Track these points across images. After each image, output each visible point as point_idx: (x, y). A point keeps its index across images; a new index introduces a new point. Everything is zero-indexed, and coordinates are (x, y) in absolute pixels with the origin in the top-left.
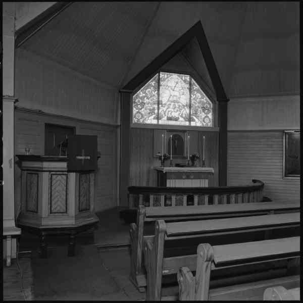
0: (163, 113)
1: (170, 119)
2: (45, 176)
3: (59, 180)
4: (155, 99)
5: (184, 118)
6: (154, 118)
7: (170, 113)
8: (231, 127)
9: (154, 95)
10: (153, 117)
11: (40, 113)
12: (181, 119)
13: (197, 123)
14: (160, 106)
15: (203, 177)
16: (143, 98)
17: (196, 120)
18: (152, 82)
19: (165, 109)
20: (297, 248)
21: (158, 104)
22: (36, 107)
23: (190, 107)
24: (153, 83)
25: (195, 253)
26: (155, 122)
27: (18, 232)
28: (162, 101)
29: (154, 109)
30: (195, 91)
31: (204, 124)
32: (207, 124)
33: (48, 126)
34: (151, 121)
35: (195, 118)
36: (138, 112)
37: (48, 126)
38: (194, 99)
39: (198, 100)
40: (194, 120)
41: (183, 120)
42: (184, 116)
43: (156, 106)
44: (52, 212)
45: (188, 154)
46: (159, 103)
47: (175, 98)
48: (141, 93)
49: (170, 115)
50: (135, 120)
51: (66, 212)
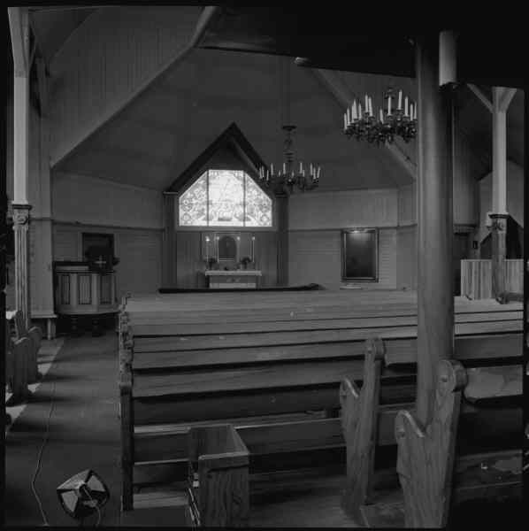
0: (213, 213)
1: (220, 219)
2: (74, 278)
3: (84, 280)
4: (205, 199)
6: (204, 219)
8: (292, 226)
12: (235, 219)
13: (253, 223)
16: (190, 199)
18: (200, 181)
20: (516, 389)
21: (208, 204)
23: (244, 205)
24: (202, 182)
26: (204, 224)
27: (55, 316)
29: (203, 210)
30: (249, 188)
32: (265, 224)
33: (85, 235)
34: (200, 222)
36: (185, 214)
37: (85, 235)
40: (249, 220)
43: (205, 207)
44: (88, 302)
45: (239, 256)
46: (208, 203)
47: (227, 197)
48: (188, 194)
49: (221, 216)
50: (182, 223)
51: (90, 304)
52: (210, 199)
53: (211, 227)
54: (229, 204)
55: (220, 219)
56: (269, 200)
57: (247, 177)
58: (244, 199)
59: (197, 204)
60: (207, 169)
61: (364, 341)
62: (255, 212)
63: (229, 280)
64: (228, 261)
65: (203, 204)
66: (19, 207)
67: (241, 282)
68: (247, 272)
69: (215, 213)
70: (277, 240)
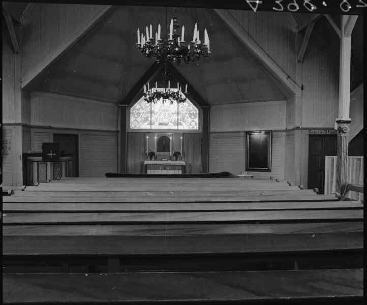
1: (160, 124)
2: (35, 164)
3: (42, 166)
4: (149, 109)
5: (173, 123)
6: (148, 124)
7: (161, 120)
8: (212, 129)
9: (148, 107)
10: (146, 123)
11: (50, 128)
14: (153, 114)
15: (152, 167)
16: (139, 109)
17: (184, 124)
19: (157, 117)
21: (151, 113)
22: (47, 125)
25: (308, 189)
26: (148, 127)
28: (154, 111)
29: (148, 117)
31: (191, 127)
32: (193, 127)
33: (55, 135)
34: (145, 126)
35: (183, 123)
38: (182, 107)
39: (185, 108)
40: (181, 124)
41: (172, 124)
42: (173, 121)
49: (161, 122)
55: (160, 124)
68: (156, 162)
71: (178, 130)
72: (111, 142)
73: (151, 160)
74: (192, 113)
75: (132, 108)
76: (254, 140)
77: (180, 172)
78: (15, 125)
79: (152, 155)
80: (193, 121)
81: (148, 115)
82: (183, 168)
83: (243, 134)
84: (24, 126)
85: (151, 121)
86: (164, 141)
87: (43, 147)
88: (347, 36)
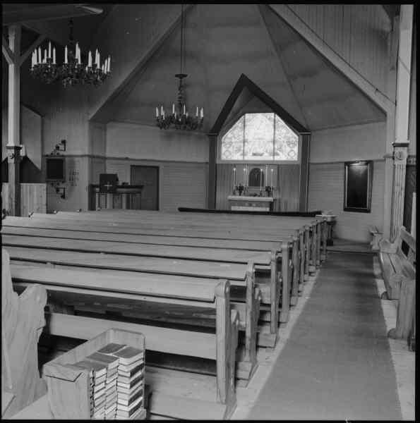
0: (248, 150)
1: (254, 154)
4: (242, 138)
6: (241, 155)
8: (314, 159)
12: (266, 154)
13: (282, 157)
14: (246, 144)
18: (239, 124)
23: (274, 142)
26: (240, 158)
30: (279, 127)
32: (292, 157)
34: (237, 157)
40: (278, 155)
43: (242, 144)
47: (260, 136)
48: (229, 134)
49: (254, 152)
50: (224, 157)
52: (246, 138)
53: (277, 161)
54: (262, 141)
55: (254, 154)
56: (297, 137)
57: (278, 118)
58: (274, 137)
59: (236, 142)
60: (244, 114)
61: (246, 263)
62: (283, 148)
63: (247, 204)
64: (254, 190)
65: (241, 142)
66: (9, 148)
67: (257, 206)
68: (243, 198)
69: (250, 150)
70: (302, 172)
71: (274, 161)
72: (202, 176)
73: (240, 195)
74: (291, 140)
75: (223, 138)
76: (359, 171)
77: (268, 210)
78: (82, 156)
79: (241, 189)
80: (292, 151)
81: (239, 144)
82: (271, 204)
83: (343, 165)
84: (91, 157)
85: (243, 151)
86: (256, 175)
87: (101, 180)
88: (406, 28)
